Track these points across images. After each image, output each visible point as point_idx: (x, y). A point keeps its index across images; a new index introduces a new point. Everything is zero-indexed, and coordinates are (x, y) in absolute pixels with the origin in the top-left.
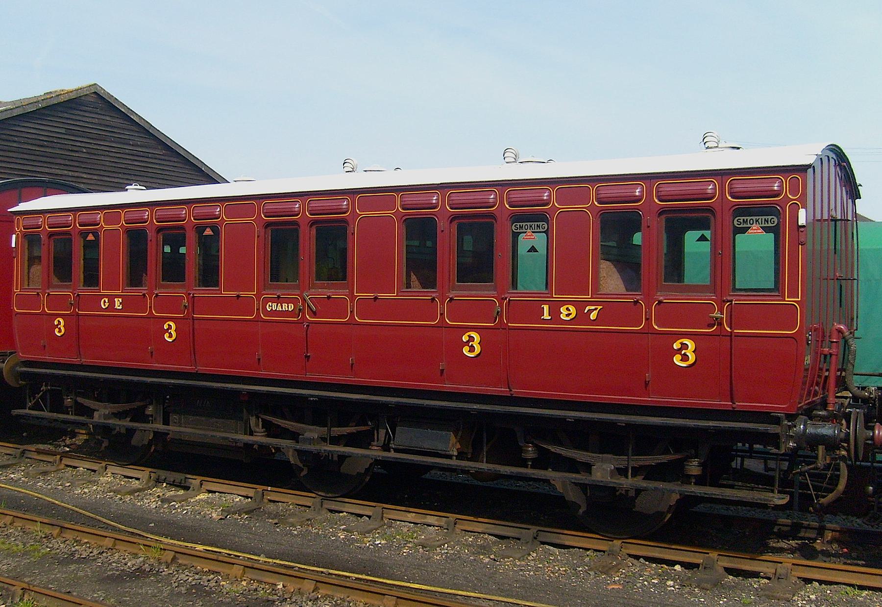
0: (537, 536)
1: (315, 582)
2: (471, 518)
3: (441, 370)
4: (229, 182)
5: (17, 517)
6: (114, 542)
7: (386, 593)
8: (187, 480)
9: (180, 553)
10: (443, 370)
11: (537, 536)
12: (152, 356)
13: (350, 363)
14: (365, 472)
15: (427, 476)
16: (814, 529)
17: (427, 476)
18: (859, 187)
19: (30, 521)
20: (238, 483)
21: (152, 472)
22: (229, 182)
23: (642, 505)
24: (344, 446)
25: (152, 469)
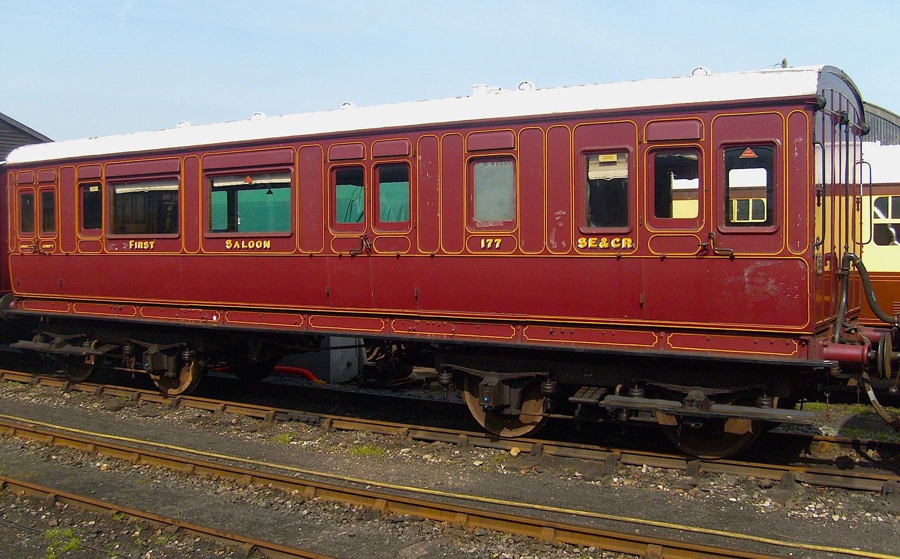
0: (621, 458)
1: (386, 501)
2: (653, 454)
3: (641, 304)
4: (54, 141)
5: (143, 454)
6: (252, 478)
7: (378, 497)
8: (321, 419)
9: (99, 445)
10: (643, 304)
11: (621, 458)
12: (417, 299)
13: (326, 292)
14: (678, 423)
15: (773, 431)
16: (850, 443)
17: (773, 431)
18: (863, 104)
19: (607, 539)
20: (394, 423)
21: (411, 429)
22: (54, 141)
23: (731, 427)
24: (732, 404)
25: (555, 442)
